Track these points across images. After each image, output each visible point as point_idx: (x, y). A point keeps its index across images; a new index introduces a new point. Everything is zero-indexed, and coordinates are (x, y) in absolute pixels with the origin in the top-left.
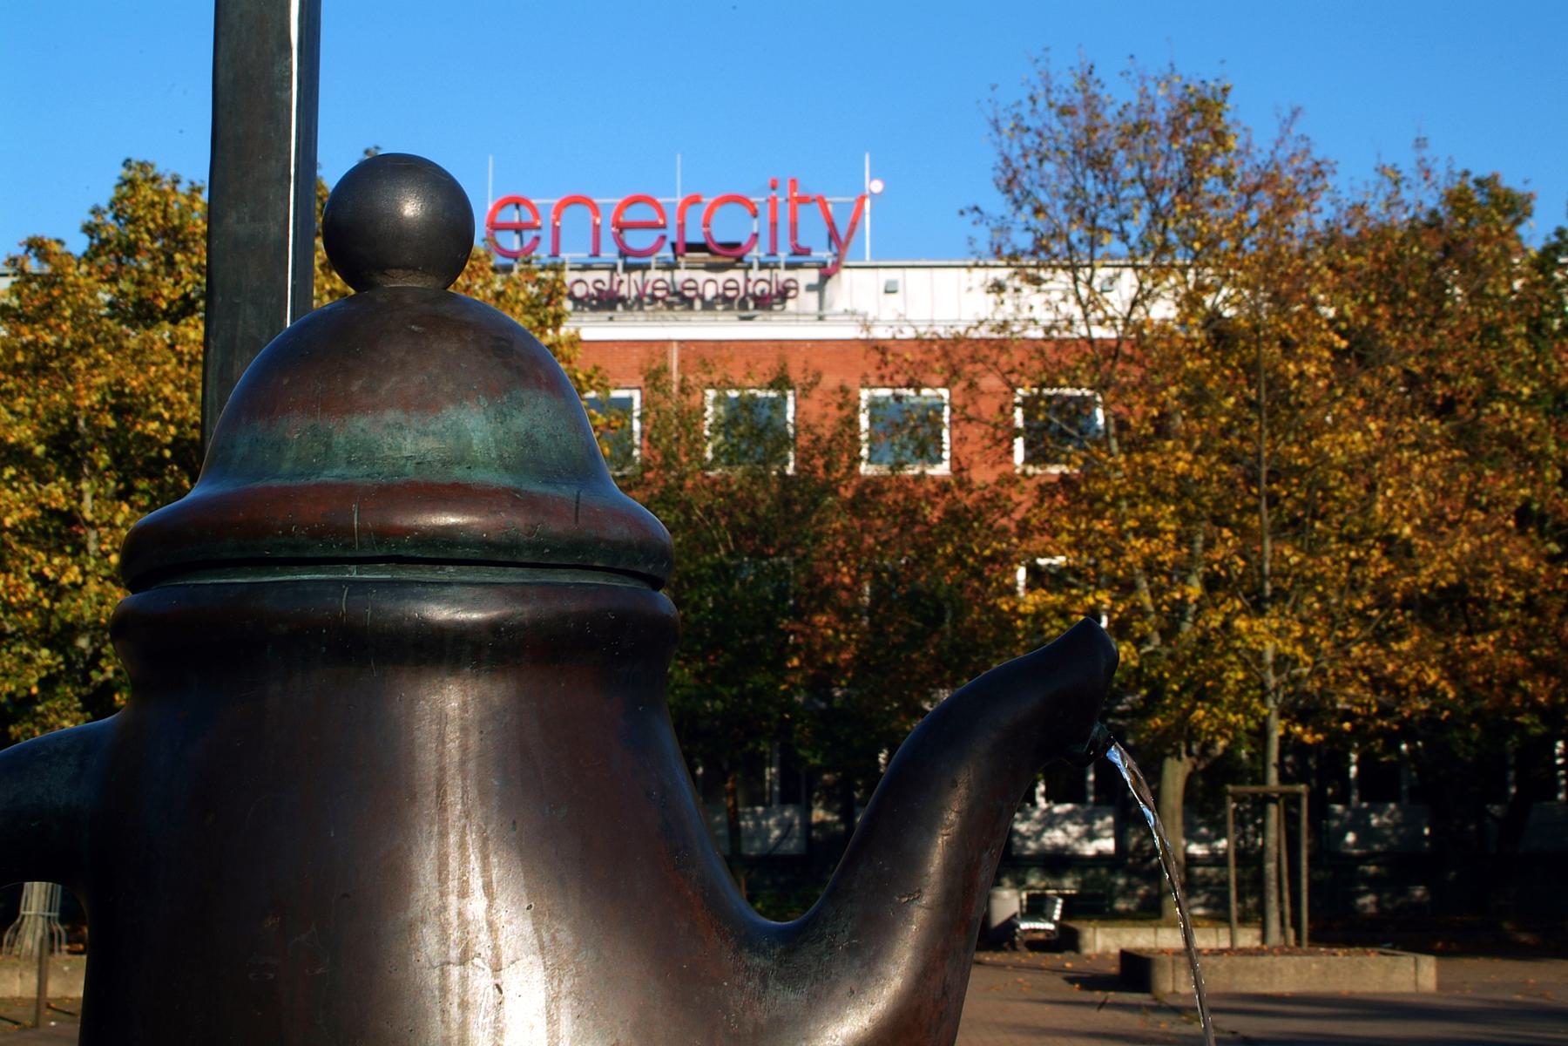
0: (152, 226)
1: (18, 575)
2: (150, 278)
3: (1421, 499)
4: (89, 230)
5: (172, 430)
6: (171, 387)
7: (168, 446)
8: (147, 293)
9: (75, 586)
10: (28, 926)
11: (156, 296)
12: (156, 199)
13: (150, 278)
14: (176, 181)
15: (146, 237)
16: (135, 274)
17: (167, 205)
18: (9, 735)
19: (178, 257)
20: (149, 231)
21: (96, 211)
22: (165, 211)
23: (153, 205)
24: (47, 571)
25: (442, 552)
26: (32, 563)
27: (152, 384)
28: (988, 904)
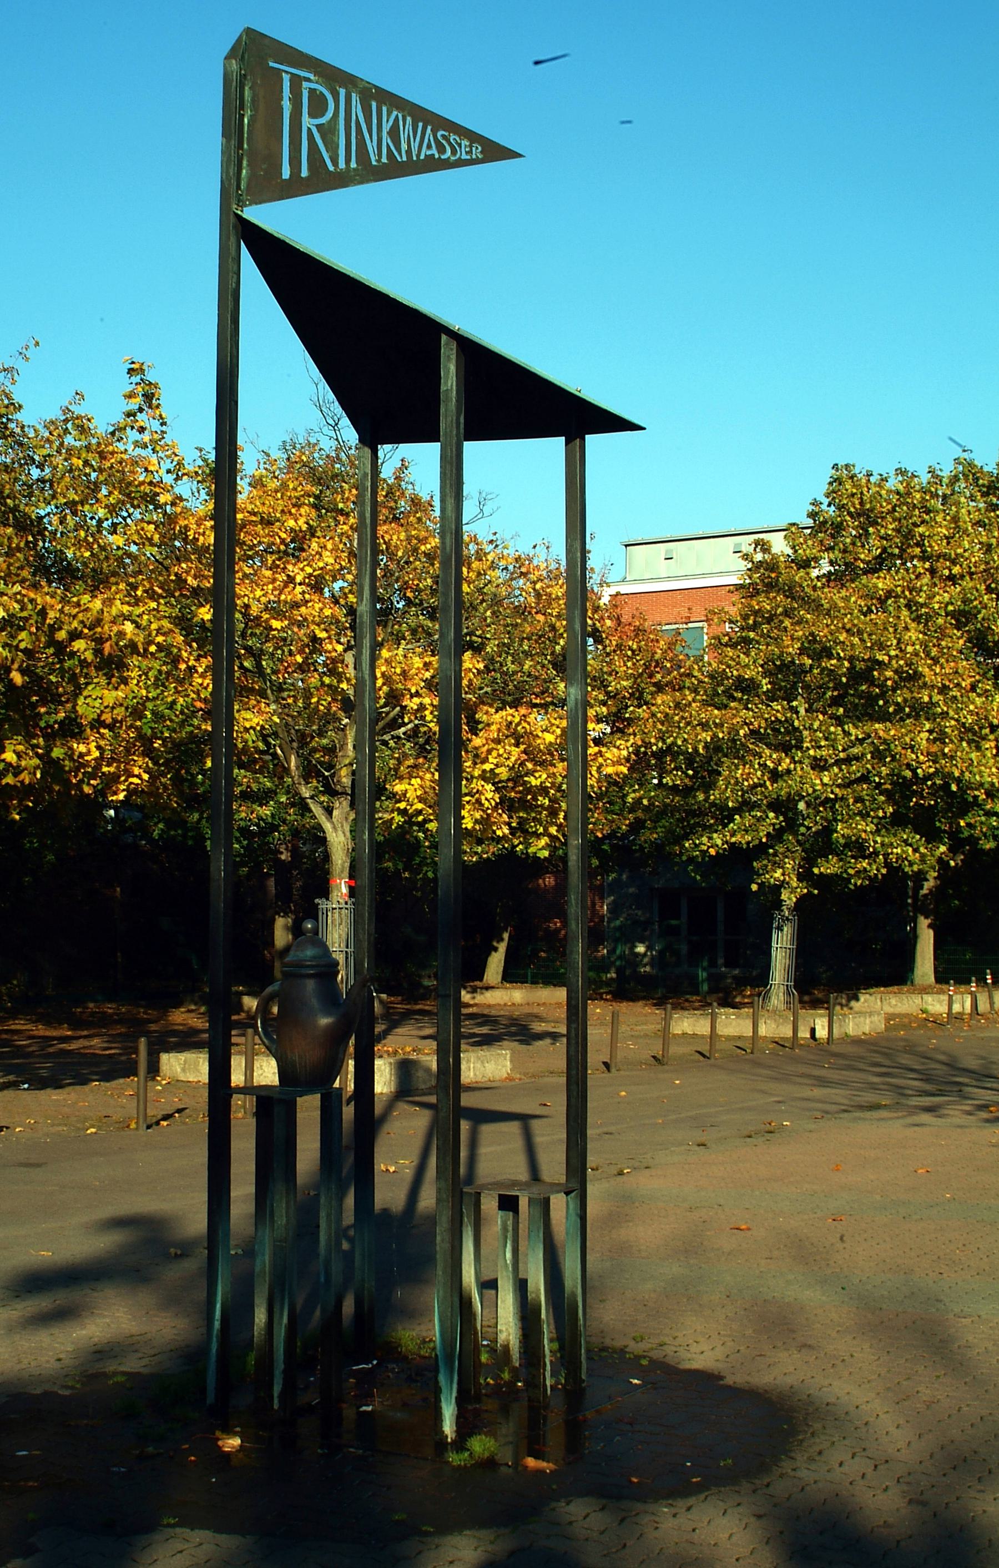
0: (852, 510)
1: (752, 766)
2: (851, 548)
3: (895, 850)
4: (812, 515)
5: (846, 664)
6: (845, 635)
7: (844, 675)
8: (850, 558)
9: (788, 771)
10: (774, 991)
11: (856, 560)
12: (854, 491)
13: (851, 548)
14: (869, 475)
15: (848, 518)
16: (841, 546)
17: (862, 493)
18: (754, 868)
19: (871, 530)
20: (850, 514)
21: (815, 503)
22: (861, 498)
23: (853, 495)
24: (768, 763)
25: (308, 966)
26: (761, 757)
27: (832, 634)
28: (644, 998)
